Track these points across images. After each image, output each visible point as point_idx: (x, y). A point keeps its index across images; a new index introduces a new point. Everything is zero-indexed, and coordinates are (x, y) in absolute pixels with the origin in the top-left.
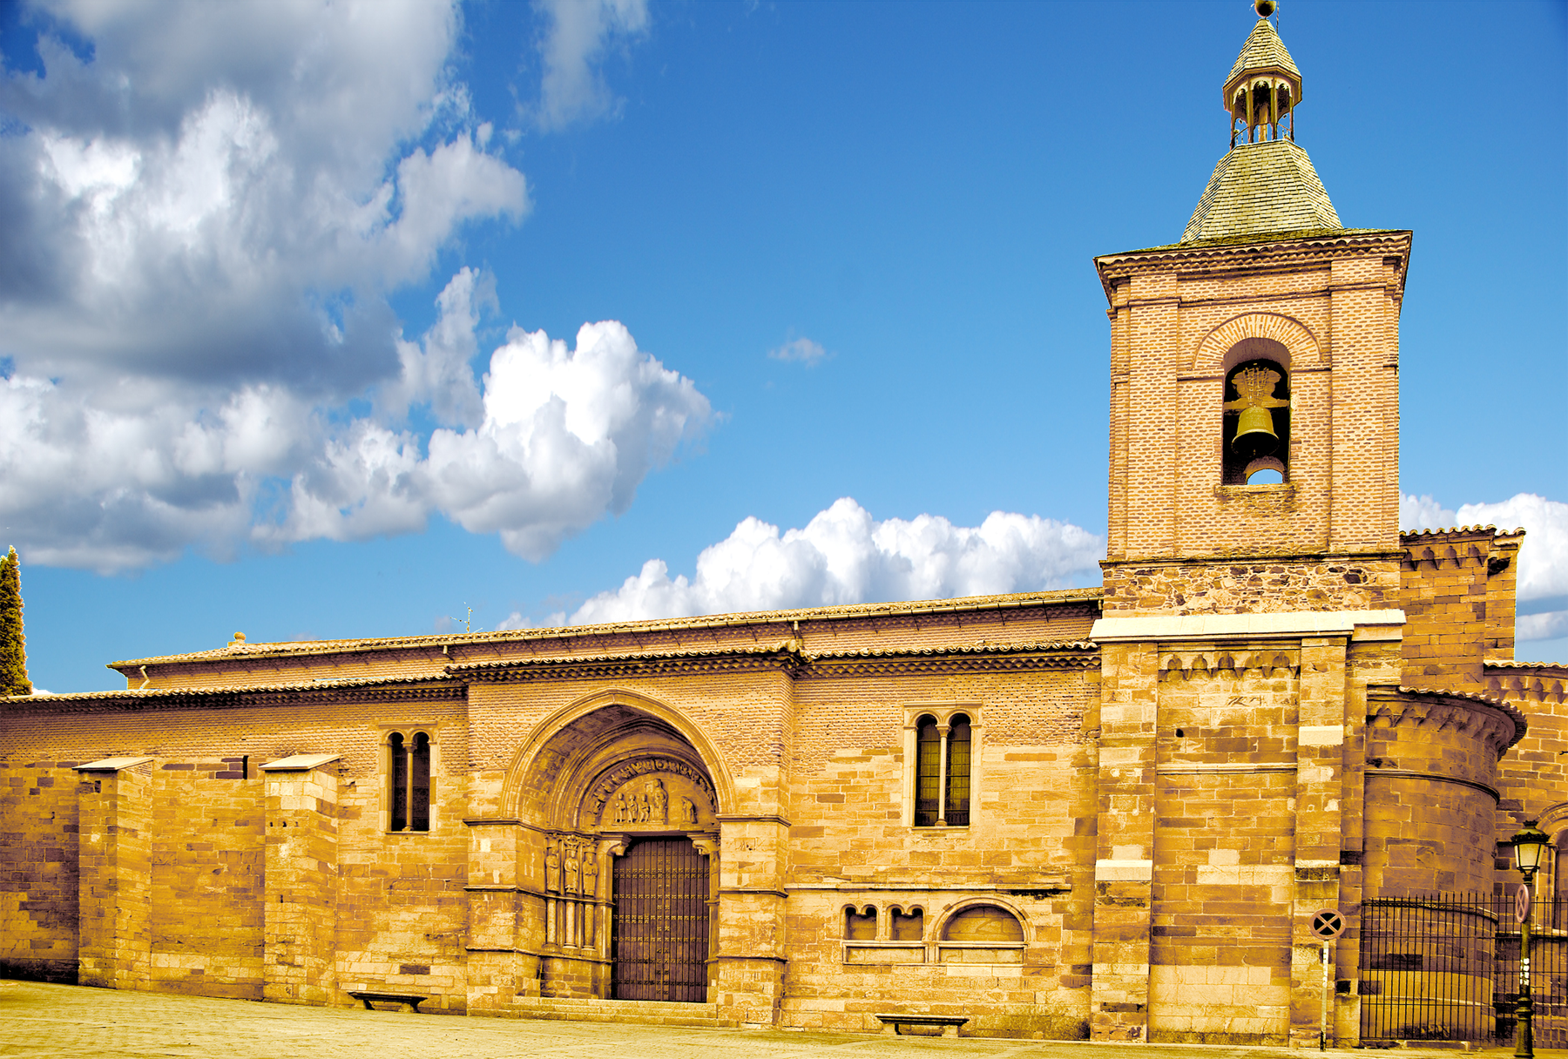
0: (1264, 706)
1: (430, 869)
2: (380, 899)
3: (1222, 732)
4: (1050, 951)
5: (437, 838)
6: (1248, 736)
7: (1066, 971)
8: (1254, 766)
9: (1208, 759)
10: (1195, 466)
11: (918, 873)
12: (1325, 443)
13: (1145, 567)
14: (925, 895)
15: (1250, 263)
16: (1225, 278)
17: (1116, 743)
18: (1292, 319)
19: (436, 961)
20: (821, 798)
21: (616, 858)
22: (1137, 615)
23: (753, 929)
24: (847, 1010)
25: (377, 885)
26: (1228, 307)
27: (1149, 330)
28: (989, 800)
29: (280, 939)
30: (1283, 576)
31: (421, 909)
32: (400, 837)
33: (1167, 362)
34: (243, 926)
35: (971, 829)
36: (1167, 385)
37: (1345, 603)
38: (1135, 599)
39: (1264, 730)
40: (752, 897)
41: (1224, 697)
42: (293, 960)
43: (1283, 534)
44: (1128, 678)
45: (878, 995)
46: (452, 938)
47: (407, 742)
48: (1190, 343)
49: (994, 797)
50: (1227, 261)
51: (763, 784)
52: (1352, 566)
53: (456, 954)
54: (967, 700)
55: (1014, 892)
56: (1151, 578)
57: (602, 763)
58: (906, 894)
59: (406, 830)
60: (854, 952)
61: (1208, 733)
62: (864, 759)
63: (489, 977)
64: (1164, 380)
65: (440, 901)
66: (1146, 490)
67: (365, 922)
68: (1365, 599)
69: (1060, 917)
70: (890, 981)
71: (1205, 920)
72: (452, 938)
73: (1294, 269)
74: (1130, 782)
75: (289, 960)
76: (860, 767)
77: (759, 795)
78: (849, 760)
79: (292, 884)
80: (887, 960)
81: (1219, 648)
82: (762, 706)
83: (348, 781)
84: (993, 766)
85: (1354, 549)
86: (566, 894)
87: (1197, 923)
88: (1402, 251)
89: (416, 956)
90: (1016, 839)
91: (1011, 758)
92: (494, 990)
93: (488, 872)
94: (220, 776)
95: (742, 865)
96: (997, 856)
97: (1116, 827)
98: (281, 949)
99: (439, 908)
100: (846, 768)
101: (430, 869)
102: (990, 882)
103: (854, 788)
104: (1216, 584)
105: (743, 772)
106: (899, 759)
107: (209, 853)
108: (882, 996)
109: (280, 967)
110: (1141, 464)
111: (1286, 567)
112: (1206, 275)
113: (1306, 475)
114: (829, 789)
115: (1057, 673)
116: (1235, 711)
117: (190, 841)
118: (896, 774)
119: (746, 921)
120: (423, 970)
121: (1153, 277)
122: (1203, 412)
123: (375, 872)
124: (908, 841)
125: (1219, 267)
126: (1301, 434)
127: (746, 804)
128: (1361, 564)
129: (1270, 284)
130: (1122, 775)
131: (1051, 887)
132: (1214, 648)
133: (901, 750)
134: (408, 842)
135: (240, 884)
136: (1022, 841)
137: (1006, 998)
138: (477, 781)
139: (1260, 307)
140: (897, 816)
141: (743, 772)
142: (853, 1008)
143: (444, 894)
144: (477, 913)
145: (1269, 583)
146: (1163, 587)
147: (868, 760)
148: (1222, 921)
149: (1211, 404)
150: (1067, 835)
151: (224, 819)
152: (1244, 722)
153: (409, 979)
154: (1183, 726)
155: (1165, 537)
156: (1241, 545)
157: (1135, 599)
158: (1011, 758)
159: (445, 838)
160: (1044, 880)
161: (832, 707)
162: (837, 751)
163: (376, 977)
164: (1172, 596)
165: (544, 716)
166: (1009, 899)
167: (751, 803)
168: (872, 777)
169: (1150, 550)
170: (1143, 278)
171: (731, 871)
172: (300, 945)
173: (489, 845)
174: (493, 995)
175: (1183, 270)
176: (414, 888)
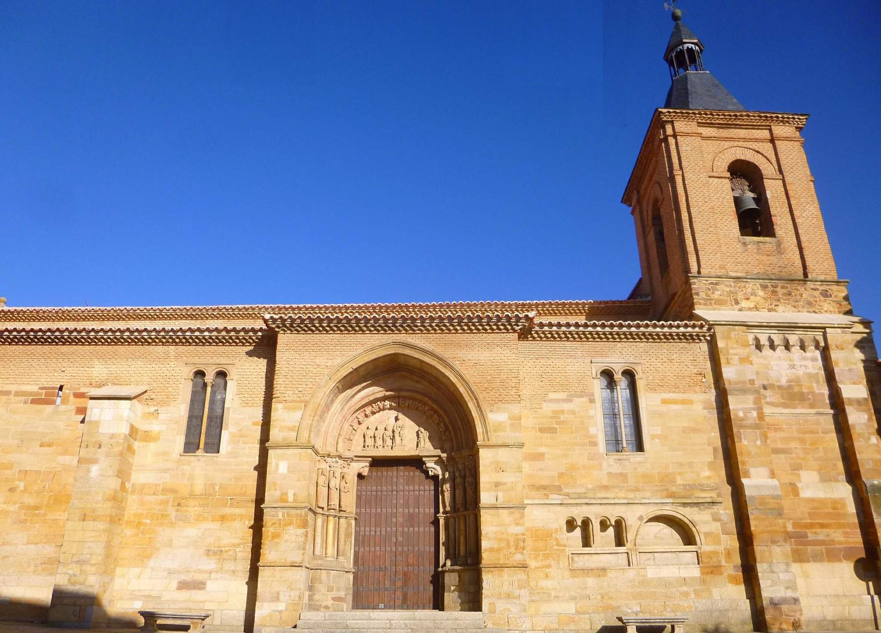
0: (808, 371)
1: (217, 488)
2: (168, 515)
3: (790, 387)
5: (226, 459)
6: (804, 390)
8: (814, 411)
9: (785, 406)
10: (725, 224)
11: (617, 490)
13: (714, 280)
14: (623, 508)
15: (732, 121)
16: (720, 128)
17: (736, 393)
18: (758, 152)
20: (541, 430)
21: (360, 476)
22: (715, 309)
23: (508, 541)
24: (578, 612)
25: (166, 502)
26: (724, 142)
29: (75, 559)
30: (788, 291)
32: (193, 459)
33: (701, 166)
34: (28, 543)
35: (646, 455)
37: (825, 309)
38: (712, 299)
39: (812, 386)
40: (506, 511)
41: (785, 364)
42: (85, 580)
43: (779, 267)
44: (733, 348)
45: (599, 597)
46: (230, 553)
47: (209, 378)
49: (658, 431)
50: (722, 119)
51: (509, 418)
52: (823, 288)
54: (632, 360)
55: (685, 505)
56: (717, 287)
57: (363, 398)
59: (200, 452)
60: (576, 558)
61: (780, 387)
62: (568, 400)
63: (278, 593)
67: (150, 538)
68: (834, 307)
69: (718, 524)
70: (606, 583)
71: (811, 526)
73: (754, 127)
76: (566, 406)
78: (558, 401)
80: (601, 565)
81: (780, 332)
82: (505, 358)
83: (152, 409)
85: (822, 278)
86: (329, 509)
87: (807, 529)
88: (804, 125)
89: (195, 572)
91: (665, 402)
92: (281, 606)
94: (34, 402)
95: (497, 485)
96: (666, 476)
97: (749, 454)
99: (221, 525)
101: (217, 488)
102: (667, 497)
103: (563, 422)
104: (754, 294)
105: (495, 408)
106: (592, 401)
107: (8, 472)
111: (789, 286)
112: (711, 125)
115: (683, 344)
116: (793, 373)
118: (592, 412)
119: (502, 534)
120: (199, 585)
121: (685, 122)
122: (723, 195)
123: (165, 491)
124: (605, 465)
125: (717, 122)
126: (776, 212)
127: (498, 434)
128: (827, 287)
129: (742, 133)
130: (745, 415)
131: (710, 500)
132: (777, 332)
133: (593, 394)
134: (201, 460)
136: (681, 464)
137: (693, 596)
138: (280, 411)
139: (740, 144)
140: (595, 444)
143: (228, 511)
144: (271, 529)
146: (726, 293)
147: (571, 401)
148: (822, 526)
150: (709, 460)
153: (185, 595)
154: (765, 383)
155: (720, 263)
156: (759, 271)
157: (712, 299)
158: (665, 402)
159: (232, 460)
160: (703, 495)
161: (543, 362)
162: (550, 394)
163: (154, 594)
164: (732, 298)
165: (339, 361)
166: (681, 510)
167: (502, 434)
169: (714, 270)
170: (680, 122)
172: (94, 565)
174: (280, 612)
175: (700, 121)
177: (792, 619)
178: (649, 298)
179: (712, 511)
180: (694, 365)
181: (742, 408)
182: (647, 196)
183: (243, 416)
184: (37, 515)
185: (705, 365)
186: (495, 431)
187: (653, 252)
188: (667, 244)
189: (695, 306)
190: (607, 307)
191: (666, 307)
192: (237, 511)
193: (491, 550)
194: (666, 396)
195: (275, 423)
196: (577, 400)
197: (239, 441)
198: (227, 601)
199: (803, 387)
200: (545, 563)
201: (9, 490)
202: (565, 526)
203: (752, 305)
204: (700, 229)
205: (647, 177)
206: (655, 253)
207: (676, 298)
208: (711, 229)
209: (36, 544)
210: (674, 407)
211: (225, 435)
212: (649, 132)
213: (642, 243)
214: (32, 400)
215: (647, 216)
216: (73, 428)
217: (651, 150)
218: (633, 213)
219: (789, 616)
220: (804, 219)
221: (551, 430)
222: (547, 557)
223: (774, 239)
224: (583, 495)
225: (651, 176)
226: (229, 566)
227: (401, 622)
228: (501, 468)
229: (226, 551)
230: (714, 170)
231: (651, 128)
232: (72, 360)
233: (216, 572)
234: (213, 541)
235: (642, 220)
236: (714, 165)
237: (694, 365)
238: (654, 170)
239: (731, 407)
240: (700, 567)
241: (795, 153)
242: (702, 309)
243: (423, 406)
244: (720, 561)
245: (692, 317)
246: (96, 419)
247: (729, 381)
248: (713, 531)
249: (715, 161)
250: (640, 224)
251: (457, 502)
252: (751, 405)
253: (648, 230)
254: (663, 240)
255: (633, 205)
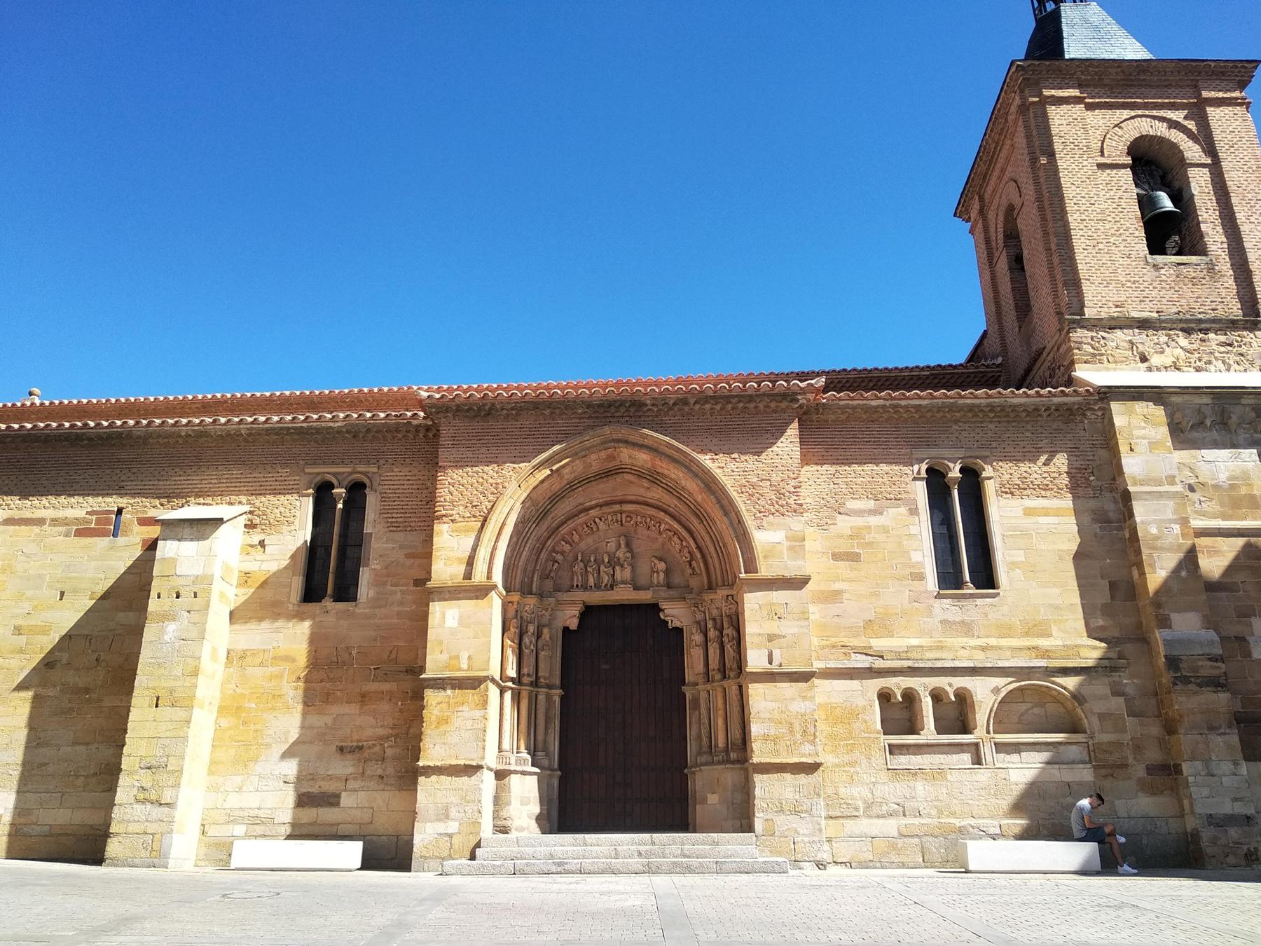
3: (1232, 487)
4: (1118, 745)
5: (367, 610)
7: (1140, 771)
12: (1229, 224)
17: (1147, 497)
19: (351, 784)
20: (836, 557)
22: (1107, 369)
24: (901, 835)
27: (1064, 122)
28: (1016, 559)
31: (336, 709)
34: (75, 743)
36: (1089, 167)
45: (934, 812)
46: (377, 749)
48: (1096, 135)
53: (379, 772)
58: (538, 706)
61: (1216, 487)
63: (447, 809)
64: (1085, 163)
65: (363, 696)
66: (1090, 255)
69: (1121, 700)
70: (945, 791)
72: (377, 749)
74: (1170, 540)
75: (153, 795)
76: (873, 521)
77: (785, 552)
79: (176, 678)
84: (1013, 521)
90: (1051, 605)
91: (1029, 512)
92: (453, 827)
93: (454, 654)
94: (79, 533)
95: (771, 638)
96: (1035, 625)
98: (146, 779)
100: (859, 521)
101: (354, 652)
103: (870, 544)
106: (914, 511)
108: (940, 813)
109: (138, 807)
110: (1081, 233)
113: (1220, 250)
114: (844, 547)
117: (20, 622)
118: (914, 530)
123: (277, 659)
126: (1205, 216)
135: (82, 680)
136: (1057, 608)
138: (446, 536)
140: (920, 577)
141: (764, 524)
142: (904, 831)
144: (436, 712)
145: (1217, 345)
149: (1125, 186)
151: (75, 591)
152: (1249, 478)
158: (1029, 512)
163: (262, 814)
168: (888, 532)
171: (759, 647)
173: (457, 618)
174: (450, 836)
176: (331, 680)
177: (1245, 848)
178: (999, 360)
179: (1111, 679)
180: (1076, 456)
181: (1155, 520)
182: (995, 203)
183: (391, 545)
184: (89, 701)
185: (1094, 455)
186: (765, 557)
187: (1006, 287)
188: (1028, 274)
189: (1076, 366)
190: (932, 375)
191: (1028, 372)
192: (385, 687)
193: (766, 738)
194: (1028, 503)
195: (438, 554)
196: (892, 512)
197: (387, 581)
198: (371, 823)
199: (1255, 487)
200: (847, 758)
201: (45, 665)
202: (877, 702)
203: (1169, 362)
204: (1083, 246)
205: (996, 173)
206: (1009, 290)
207: (1045, 354)
208: (1101, 246)
209: (87, 744)
210: (1043, 520)
211: (365, 576)
212: (1000, 100)
213: (987, 276)
214: (76, 529)
215: (996, 232)
216: (139, 571)
217: (1002, 129)
218: (971, 231)
219: (1241, 844)
220: (1253, 225)
221: (853, 557)
222: (851, 749)
223: (1204, 258)
224: (904, 655)
225: (1003, 171)
226: (375, 769)
227: (632, 848)
228: (776, 614)
229: (370, 748)
230: (1106, 154)
231: (1003, 94)
232: (134, 470)
233: (355, 779)
234: (349, 732)
235: (988, 241)
236: (1105, 146)
237: (1076, 456)
238: (1008, 160)
239: (1138, 519)
240: (1094, 767)
241: (1238, 123)
242: (1088, 370)
243: (657, 525)
244: (1127, 758)
245: (1070, 381)
246: (171, 555)
247: (1134, 478)
248: (1114, 711)
249: (1107, 140)
250: (984, 247)
251: (711, 667)
252: (1170, 515)
253: (997, 255)
254: (1022, 269)
255: (972, 220)
